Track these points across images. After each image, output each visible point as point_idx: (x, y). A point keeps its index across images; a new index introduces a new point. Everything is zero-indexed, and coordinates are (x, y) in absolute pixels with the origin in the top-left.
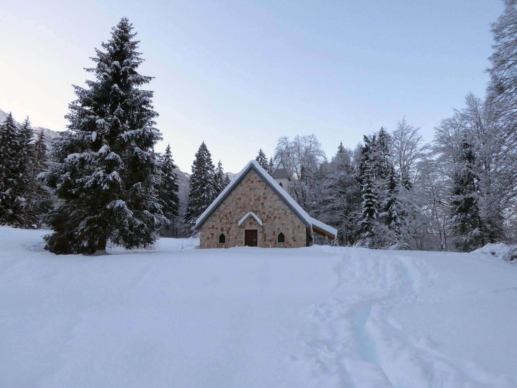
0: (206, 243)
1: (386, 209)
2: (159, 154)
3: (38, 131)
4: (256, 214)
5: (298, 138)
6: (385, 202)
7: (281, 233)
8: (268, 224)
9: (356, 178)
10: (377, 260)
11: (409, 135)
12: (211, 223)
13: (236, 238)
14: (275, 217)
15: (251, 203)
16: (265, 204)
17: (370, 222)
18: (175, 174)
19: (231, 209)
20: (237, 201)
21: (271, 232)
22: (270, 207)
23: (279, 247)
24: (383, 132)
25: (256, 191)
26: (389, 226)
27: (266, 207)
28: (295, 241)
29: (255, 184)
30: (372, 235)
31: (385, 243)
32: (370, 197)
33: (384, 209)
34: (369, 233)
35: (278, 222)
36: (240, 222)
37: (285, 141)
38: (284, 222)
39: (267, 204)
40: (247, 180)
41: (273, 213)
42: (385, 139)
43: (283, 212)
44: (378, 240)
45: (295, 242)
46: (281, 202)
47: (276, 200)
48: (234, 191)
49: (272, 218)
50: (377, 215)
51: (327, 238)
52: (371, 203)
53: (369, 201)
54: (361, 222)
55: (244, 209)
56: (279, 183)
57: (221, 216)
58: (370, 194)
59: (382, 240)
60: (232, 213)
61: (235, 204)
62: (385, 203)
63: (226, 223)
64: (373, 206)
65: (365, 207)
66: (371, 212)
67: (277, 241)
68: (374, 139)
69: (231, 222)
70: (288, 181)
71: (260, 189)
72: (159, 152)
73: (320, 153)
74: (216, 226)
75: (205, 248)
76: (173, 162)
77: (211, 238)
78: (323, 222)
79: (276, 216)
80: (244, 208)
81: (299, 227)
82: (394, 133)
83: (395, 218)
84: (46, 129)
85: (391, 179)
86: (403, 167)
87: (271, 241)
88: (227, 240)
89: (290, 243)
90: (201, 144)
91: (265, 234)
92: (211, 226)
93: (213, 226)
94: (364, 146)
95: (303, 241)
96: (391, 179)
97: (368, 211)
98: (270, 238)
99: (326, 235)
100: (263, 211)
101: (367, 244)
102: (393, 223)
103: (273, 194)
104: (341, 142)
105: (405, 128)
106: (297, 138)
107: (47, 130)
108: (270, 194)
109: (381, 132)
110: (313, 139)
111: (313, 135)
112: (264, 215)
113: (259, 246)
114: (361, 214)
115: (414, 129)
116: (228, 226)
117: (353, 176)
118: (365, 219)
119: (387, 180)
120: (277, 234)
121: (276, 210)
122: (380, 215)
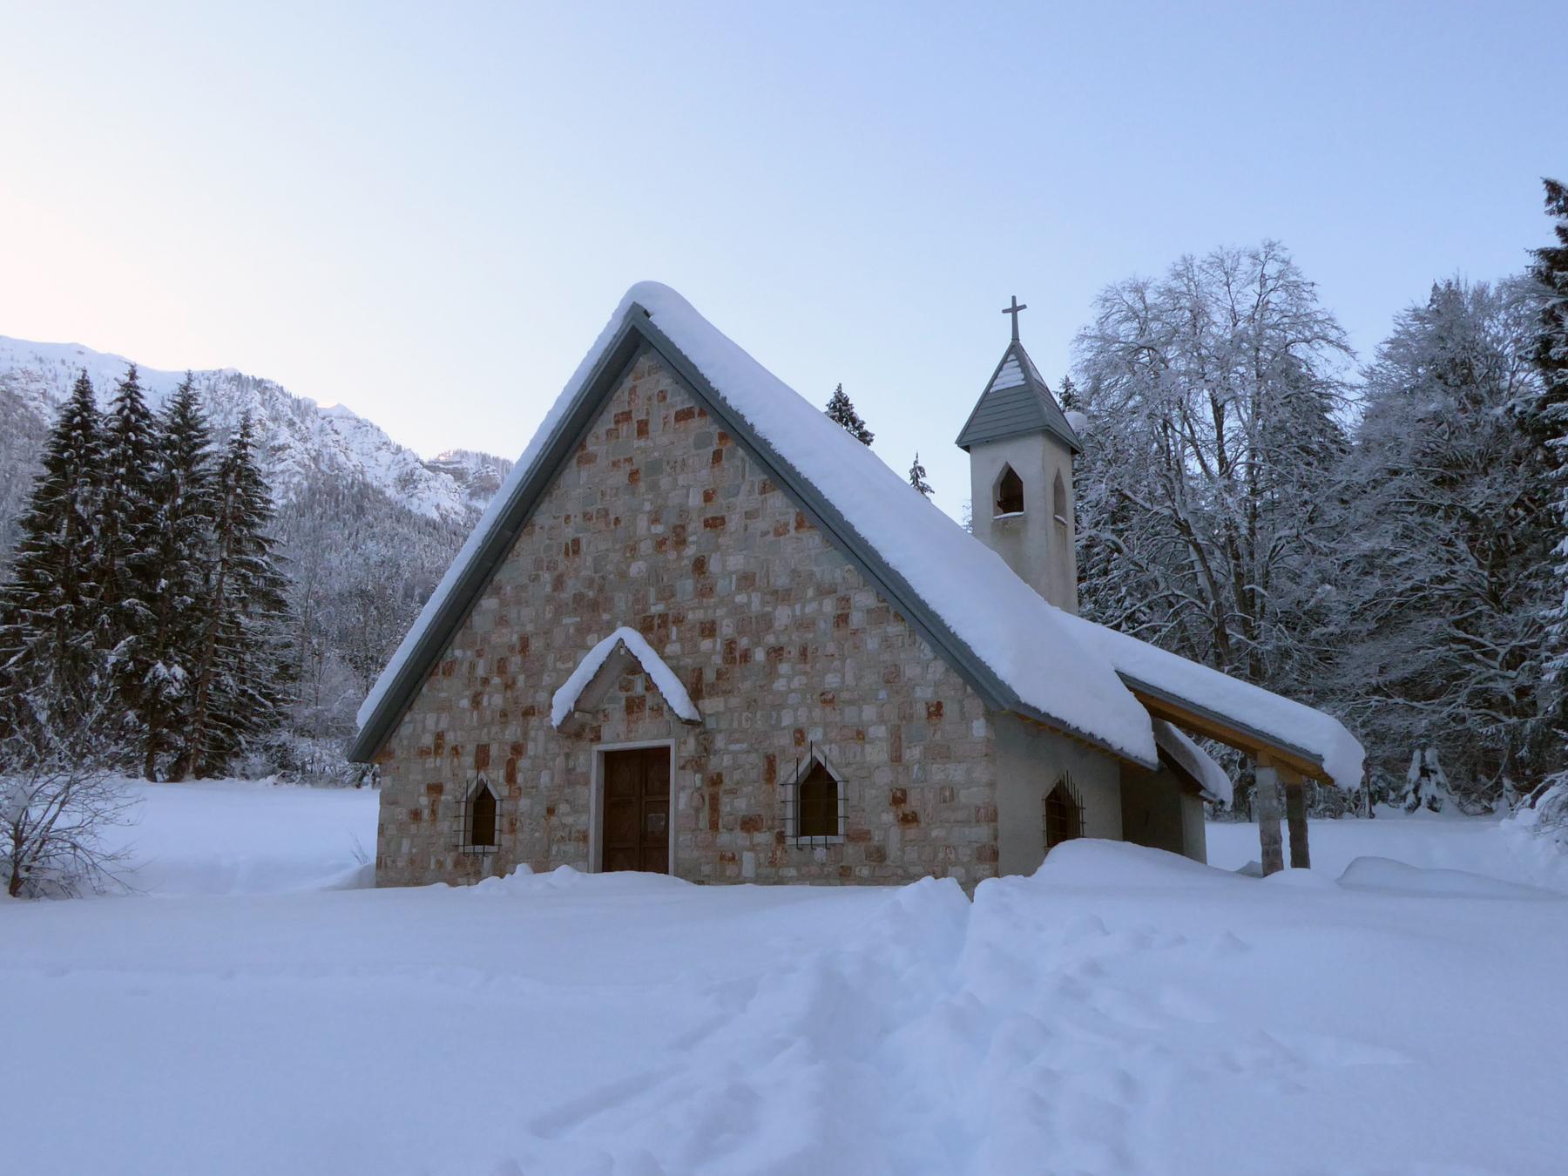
4: (659, 646)
8: (734, 701)
9: (1521, 423)
12: (430, 720)
14: (776, 653)
15: (637, 568)
16: (714, 566)
20: (563, 564)
25: (665, 482)
27: (722, 586)
28: (908, 819)
36: (563, 701)
38: (832, 681)
39: (728, 563)
40: (617, 422)
41: (766, 622)
43: (829, 606)
45: (912, 832)
46: (813, 540)
47: (780, 531)
48: (544, 507)
49: (759, 655)
60: (536, 645)
61: (548, 589)
63: (504, 714)
67: (790, 829)
74: (450, 738)
77: (426, 813)
79: (784, 639)
80: (594, 606)
81: (936, 710)
87: (749, 824)
88: (505, 822)
89: (877, 837)
91: (716, 781)
92: (428, 740)
93: (440, 736)
95: (965, 823)
103: (763, 491)
106: (1185, 270)
110: (1272, 269)
112: (706, 645)
116: (512, 732)
117: (1500, 411)
120: (789, 773)
121: (782, 596)
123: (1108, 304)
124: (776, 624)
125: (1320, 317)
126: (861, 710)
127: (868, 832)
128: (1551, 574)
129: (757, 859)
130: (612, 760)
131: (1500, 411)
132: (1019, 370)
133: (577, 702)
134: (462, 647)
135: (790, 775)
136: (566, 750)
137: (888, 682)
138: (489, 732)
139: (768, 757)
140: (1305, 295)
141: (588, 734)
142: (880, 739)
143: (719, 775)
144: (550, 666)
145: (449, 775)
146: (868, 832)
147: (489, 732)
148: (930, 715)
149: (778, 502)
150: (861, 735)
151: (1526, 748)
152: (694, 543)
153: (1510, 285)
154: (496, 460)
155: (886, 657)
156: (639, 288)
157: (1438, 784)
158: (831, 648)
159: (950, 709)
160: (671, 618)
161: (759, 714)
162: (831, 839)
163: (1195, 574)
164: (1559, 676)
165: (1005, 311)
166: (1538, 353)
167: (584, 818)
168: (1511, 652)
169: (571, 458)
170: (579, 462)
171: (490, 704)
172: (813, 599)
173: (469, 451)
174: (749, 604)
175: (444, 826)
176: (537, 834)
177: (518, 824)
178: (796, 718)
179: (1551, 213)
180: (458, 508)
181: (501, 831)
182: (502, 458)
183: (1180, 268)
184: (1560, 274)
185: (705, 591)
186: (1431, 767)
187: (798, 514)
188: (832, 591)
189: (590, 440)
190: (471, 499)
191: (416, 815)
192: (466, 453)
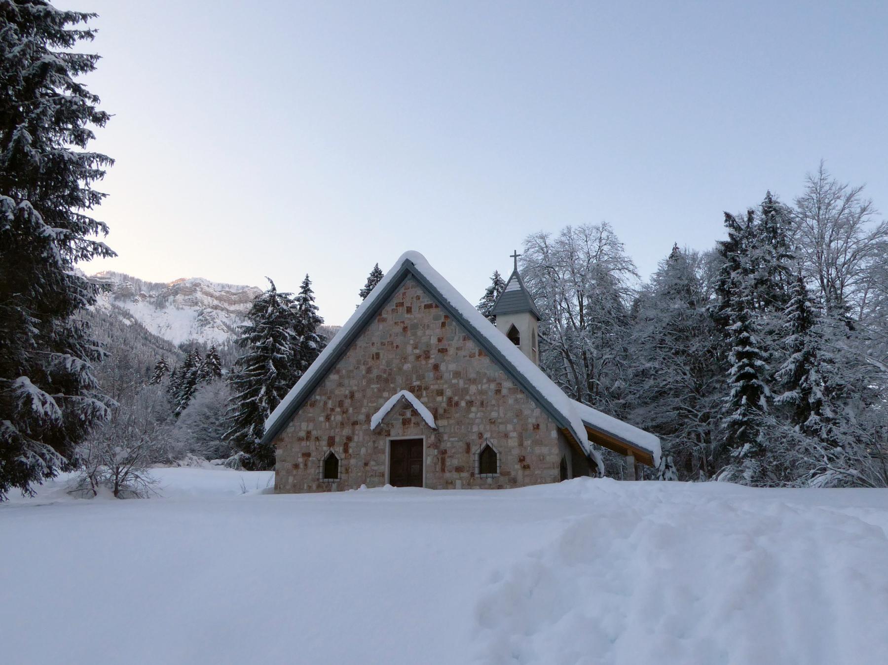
0: (291, 479)
1: (792, 384)
2: (288, 294)
3: (106, 278)
4: (419, 397)
5: (569, 232)
6: (789, 365)
7: (488, 447)
8: (452, 421)
9: (712, 316)
10: (762, 541)
11: (840, 203)
12: (304, 426)
13: (366, 464)
14: (470, 403)
15: (407, 367)
16: (443, 367)
17: (752, 417)
18: (320, 337)
19: (353, 384)
20: (371, 363)
21: (461, 444)
22: (457, 374)
23: (483, 486)
24: (770, 202)
25: (419, 333)
26: (802, 428)
27: (446, 376)
28: (526, 467)
29: (417, 315)
30: (760, 452)
31: (795, 471)
32: (750, 355)
33: (787, 383)
34: (751, 448)
35: (479, 415)
36: (376, 419)
37: (543, 245)
38: (494, 415)
39: (448, 367)
40: (397, 306)
41: (466, 391)
42: (778, 219)
43: (493, 386)
44: (775, 463)
45: (527, 472)
46: (486, 361)
47: (472, 356)
48: (362, 338)
49: (463, 404)
50: (769, 400)
51: (631, 459)
52: (751, 370)
53: (747, 365)
54: (728, 419)
55: (387, 383)
56: (507, 327)
57: (330, 404)
58: (748, 348)
59: (787, 464)
60: (358, 396)
61: (364, 372)
62: (788, 368)
63: (342, 424)
64: (757, 378)
65: (737, 380)
66: (752, 393)
67: (477, 471)
68: (750, 219)
69: (355, 419)
70: (533, 321)
71: (428, 326)
72: (286, 292)
73: (624, 265)
74: (314, 433)
75: (288, 492)
76: (316, 311)
77: (301, 466)
78: (640, 426)
79: (473, 398)
80: (387, 381)
81: (537, 427)
82: (800, 203)
83: (819, 403)
84: (121, 275)
85: (801, 307)
86: (828, 281)
87: (459, 469)
88: (343, 469)
89: (513, 474)
90: (372, 270)
91: (444, 452)
92: (302, 434)
93: (309, 433)
94: (727, 239)
95: (549, 468)
96: (801, 307)
97: (743, 391)
98: (455, 462)
99: (629, 452)
100: (436, 387)
101: (747, 474)
102: (813, 417)
103: (464, 339)
104: (676, 244)
105: (827, 188)
106: (567, 233)
107: (123, 277)
108: (456, 339)
109: (765, 202)
110: (604, 235)
111: (604, 225)
112: (439, 399)
113: (427, 487)
114: (728, 398)
115: (848, 191)
116: (347, 431)
117: (703, 310)
118: (739, 411)
119: (790, 309)
120: (476, 450)
121: (473, 381)
122: (776, 399)
123: (530, 244)
124: (470, 392)
125: (626, 260)
126: (506, 426)
127: (510, 472)
128: (724, 382)
129: (462, 483)
130: (393, 443)
131: (703, 310)
132: (518, 283)
133: (383, 419)
134: (320, 395)
135: (476, 451)
136: (374, 439)
137: (517, 416)
138: (335, 431)
139: (467, 444)
140: (619, 248)
141: (384, 433)
142: (514, 437)
143: (446, 451)
144: (365, 404)
145: (314, 449)
146: (510, 472)
147: (335, 431)
148: (534, 428)
149: (470, 345)
150: (506, 436)
151: (711, 456)
152: (433, 358)
153: (706, 255)
154: (132, 278)
155: (517, 407)
156: (407, 253)
157: (673, 472)
158: (494, 402)
159: (542, 426)
160: (423, 388)
161: (463, 427)
162: (495, 475)
163: (567, 373)
164: (728, 425)
165: (511, 256)
166: (720, 286)
167: (383, 467)
168: (704, 415)
169: (375, 319)
170: (378, 321)
171: (335, 420)
172: (486, 383)
173: (116, 272)
174: (458, 384)
175: (312, 471)
176: (359, 474)
177: (350, 470)
178: (479, 428)
179: (727, 226)
180: (107, 305)
181: (341, 472)
182: (136, 277)
183: (565, 232)
184: (730, 253)
185: (439, 378)
186: (670, 465)
187: (479, 350)
188: (494, 380)
189: (384, 312)
190: (115, 301)
191: (296, 466)
192: (114, 273)
